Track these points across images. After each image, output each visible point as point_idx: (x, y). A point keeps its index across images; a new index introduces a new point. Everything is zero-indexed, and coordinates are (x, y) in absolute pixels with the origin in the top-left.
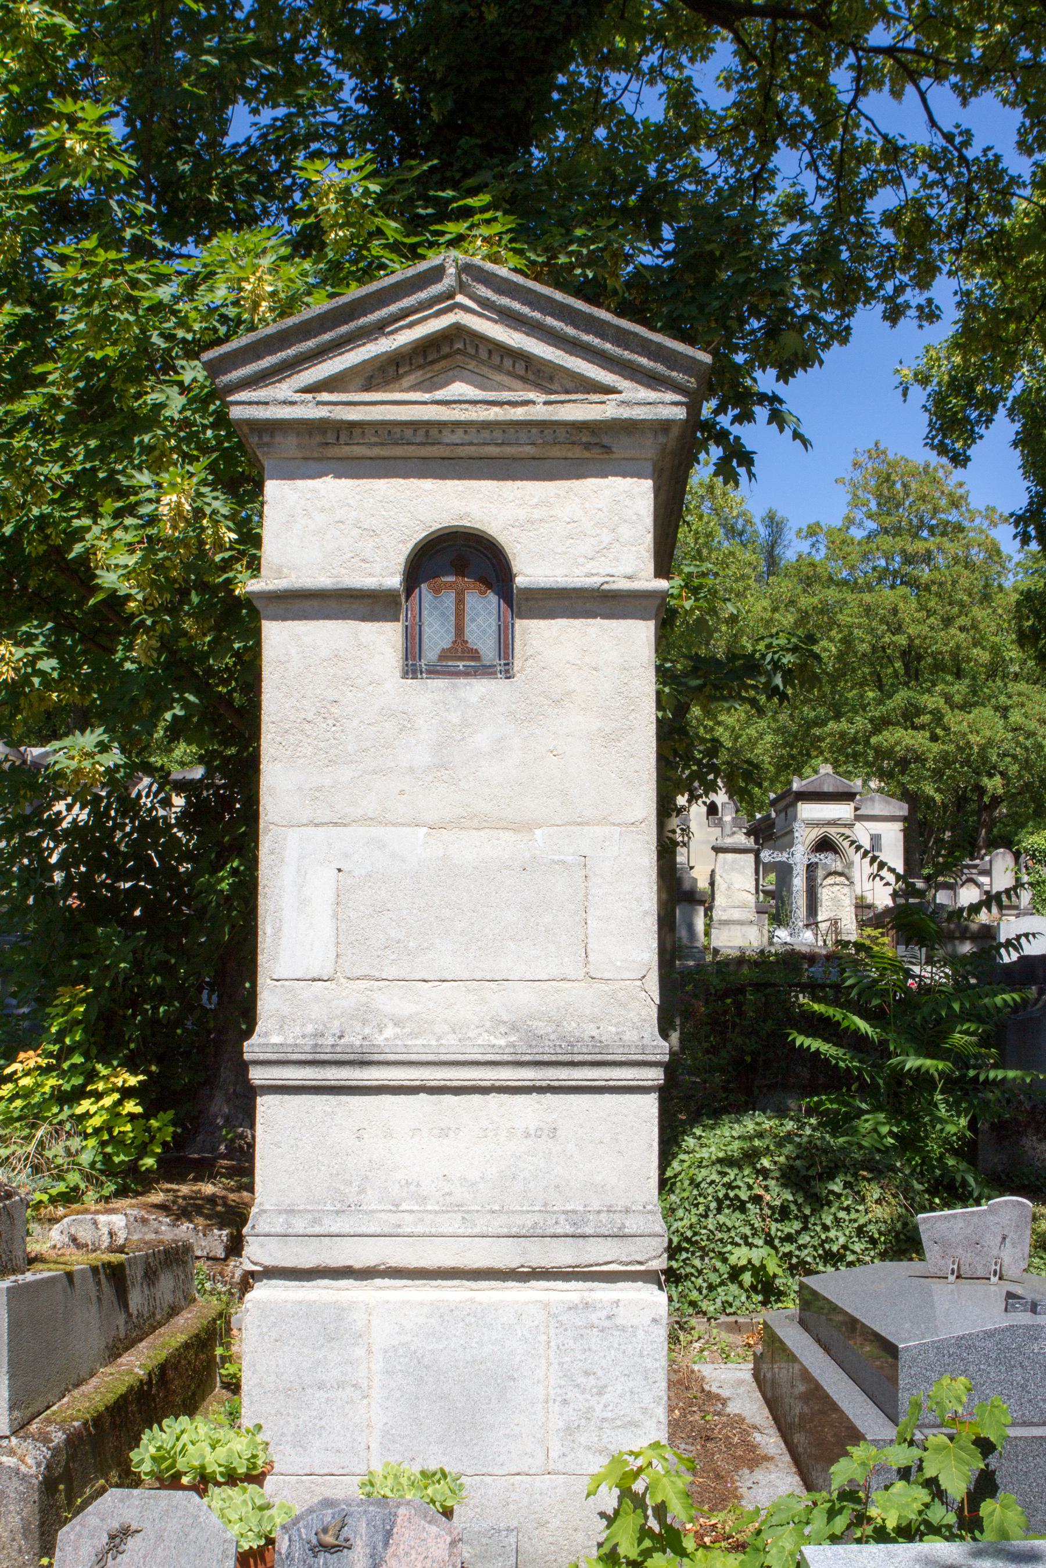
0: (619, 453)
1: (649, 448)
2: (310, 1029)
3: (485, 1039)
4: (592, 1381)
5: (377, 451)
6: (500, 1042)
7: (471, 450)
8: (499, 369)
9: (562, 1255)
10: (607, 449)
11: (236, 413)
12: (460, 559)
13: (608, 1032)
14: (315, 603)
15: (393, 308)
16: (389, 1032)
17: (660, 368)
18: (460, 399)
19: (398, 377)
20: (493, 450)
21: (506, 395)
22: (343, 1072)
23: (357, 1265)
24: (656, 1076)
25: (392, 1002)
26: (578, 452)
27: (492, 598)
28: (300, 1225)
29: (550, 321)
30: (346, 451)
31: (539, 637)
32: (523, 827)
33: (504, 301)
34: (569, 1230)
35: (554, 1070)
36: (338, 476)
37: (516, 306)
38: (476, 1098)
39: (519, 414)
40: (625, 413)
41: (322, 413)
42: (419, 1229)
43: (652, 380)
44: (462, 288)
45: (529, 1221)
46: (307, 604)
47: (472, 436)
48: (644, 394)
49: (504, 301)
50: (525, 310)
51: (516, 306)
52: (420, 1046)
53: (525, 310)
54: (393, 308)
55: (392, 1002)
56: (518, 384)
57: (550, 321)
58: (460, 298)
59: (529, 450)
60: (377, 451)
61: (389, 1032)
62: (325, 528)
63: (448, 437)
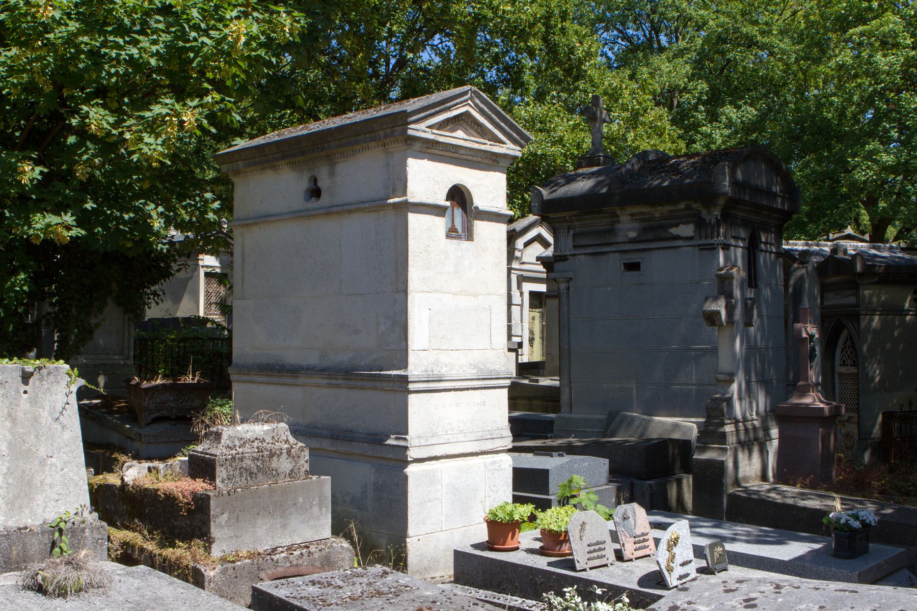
0: (501, 164)
1: (506, 163)
2: (423, 369)
3: (469, 371)
4: (495, 488)
5: (441, 153)
6: (471, 373)
7: (465, 157)
8: (472, 128)
9: (488, 446)
10: (498, 162)
11: (410, 132)
12: (458, 195)
13: (497, 367)
14: (429, 209)
15: (454, 102)
16: (444, 369)
17: (518, 138)
18: (459, 137)
19: (445, 127)
20: (470, 158)
21: (477, 140)
22: (435, 385)
23: (439, 455)
24: (411, 387)
25: (445, 358)
26: (491, 162)
27: (460, 210)
28: (423, 442)
29: (493, 116)
30: (436, 152)
31: (480, 227)
32: (476, 295)
33: (482, 106)
34: (489, 437)
35: (485, 382)
36: (429, 160)
37: (485, 108)
38: (466, 392)
39: (483, 147)
40: (508, 152)
41: (432, 137)
42: (454, 440)
43: (515, 142)
44: (471, 98)
45: (480, 434)
46: (421, 208)
47: (467, 152)
48: (512, 146)
49: (482, 106)
50: (487, 110)
51: (485, 108)
52: (454, 374)
53: (487, 110)
54: (454, 102)
55: (445, 358)
56: (476, 135)
57: (493, 116)
58: (469, 102)
59: (479, 159)
60: (441, 153)
61: (444, 369)
62: (426, 179)
63: (461, 152)
